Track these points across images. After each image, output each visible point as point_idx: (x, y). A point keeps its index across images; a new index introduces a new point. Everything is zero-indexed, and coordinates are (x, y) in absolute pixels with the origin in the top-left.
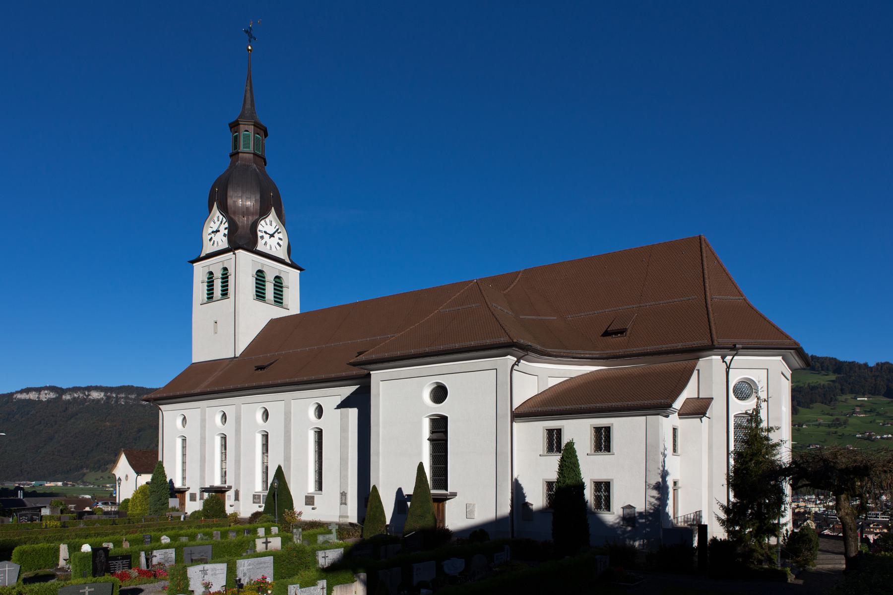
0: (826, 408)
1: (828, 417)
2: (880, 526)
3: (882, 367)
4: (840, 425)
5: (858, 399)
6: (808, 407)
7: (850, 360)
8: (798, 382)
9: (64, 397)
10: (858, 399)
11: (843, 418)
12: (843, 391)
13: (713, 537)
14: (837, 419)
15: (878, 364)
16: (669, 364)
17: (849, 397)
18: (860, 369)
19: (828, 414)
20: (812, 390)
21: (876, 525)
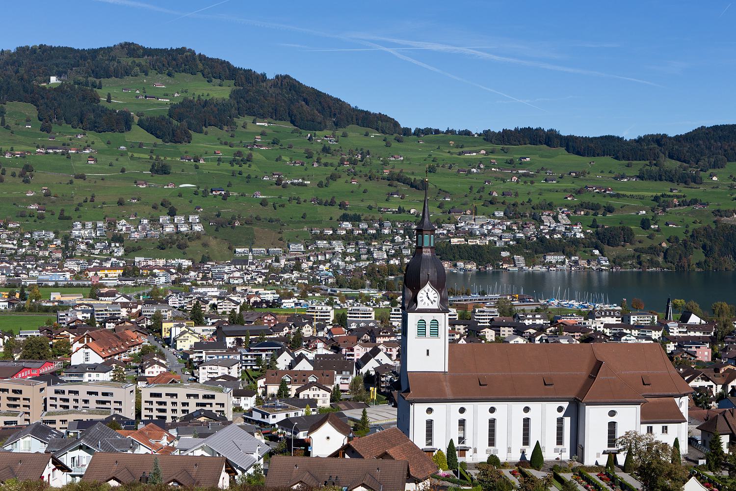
0: (224, 133)
1: (227, 147)
2: (389, 334)
3: (282, 81)
4: (245, 161)
5: (257, 124)
6: (201, 132)
7: (246, 67)
8: (186, 92)
9: (369, 325)
10: (257, 124)
11: (246, 152)
12: (240, 113)
13: (597, 463)
14: (239, 153)
15: (277, 77)
16: (450, 47)
17: (248, 119)
18: (257, 82)
19: (226, 144)
20: (204, 107)
21: (385, 333)
